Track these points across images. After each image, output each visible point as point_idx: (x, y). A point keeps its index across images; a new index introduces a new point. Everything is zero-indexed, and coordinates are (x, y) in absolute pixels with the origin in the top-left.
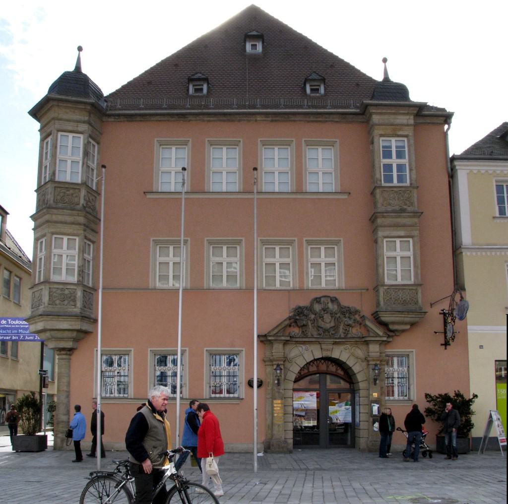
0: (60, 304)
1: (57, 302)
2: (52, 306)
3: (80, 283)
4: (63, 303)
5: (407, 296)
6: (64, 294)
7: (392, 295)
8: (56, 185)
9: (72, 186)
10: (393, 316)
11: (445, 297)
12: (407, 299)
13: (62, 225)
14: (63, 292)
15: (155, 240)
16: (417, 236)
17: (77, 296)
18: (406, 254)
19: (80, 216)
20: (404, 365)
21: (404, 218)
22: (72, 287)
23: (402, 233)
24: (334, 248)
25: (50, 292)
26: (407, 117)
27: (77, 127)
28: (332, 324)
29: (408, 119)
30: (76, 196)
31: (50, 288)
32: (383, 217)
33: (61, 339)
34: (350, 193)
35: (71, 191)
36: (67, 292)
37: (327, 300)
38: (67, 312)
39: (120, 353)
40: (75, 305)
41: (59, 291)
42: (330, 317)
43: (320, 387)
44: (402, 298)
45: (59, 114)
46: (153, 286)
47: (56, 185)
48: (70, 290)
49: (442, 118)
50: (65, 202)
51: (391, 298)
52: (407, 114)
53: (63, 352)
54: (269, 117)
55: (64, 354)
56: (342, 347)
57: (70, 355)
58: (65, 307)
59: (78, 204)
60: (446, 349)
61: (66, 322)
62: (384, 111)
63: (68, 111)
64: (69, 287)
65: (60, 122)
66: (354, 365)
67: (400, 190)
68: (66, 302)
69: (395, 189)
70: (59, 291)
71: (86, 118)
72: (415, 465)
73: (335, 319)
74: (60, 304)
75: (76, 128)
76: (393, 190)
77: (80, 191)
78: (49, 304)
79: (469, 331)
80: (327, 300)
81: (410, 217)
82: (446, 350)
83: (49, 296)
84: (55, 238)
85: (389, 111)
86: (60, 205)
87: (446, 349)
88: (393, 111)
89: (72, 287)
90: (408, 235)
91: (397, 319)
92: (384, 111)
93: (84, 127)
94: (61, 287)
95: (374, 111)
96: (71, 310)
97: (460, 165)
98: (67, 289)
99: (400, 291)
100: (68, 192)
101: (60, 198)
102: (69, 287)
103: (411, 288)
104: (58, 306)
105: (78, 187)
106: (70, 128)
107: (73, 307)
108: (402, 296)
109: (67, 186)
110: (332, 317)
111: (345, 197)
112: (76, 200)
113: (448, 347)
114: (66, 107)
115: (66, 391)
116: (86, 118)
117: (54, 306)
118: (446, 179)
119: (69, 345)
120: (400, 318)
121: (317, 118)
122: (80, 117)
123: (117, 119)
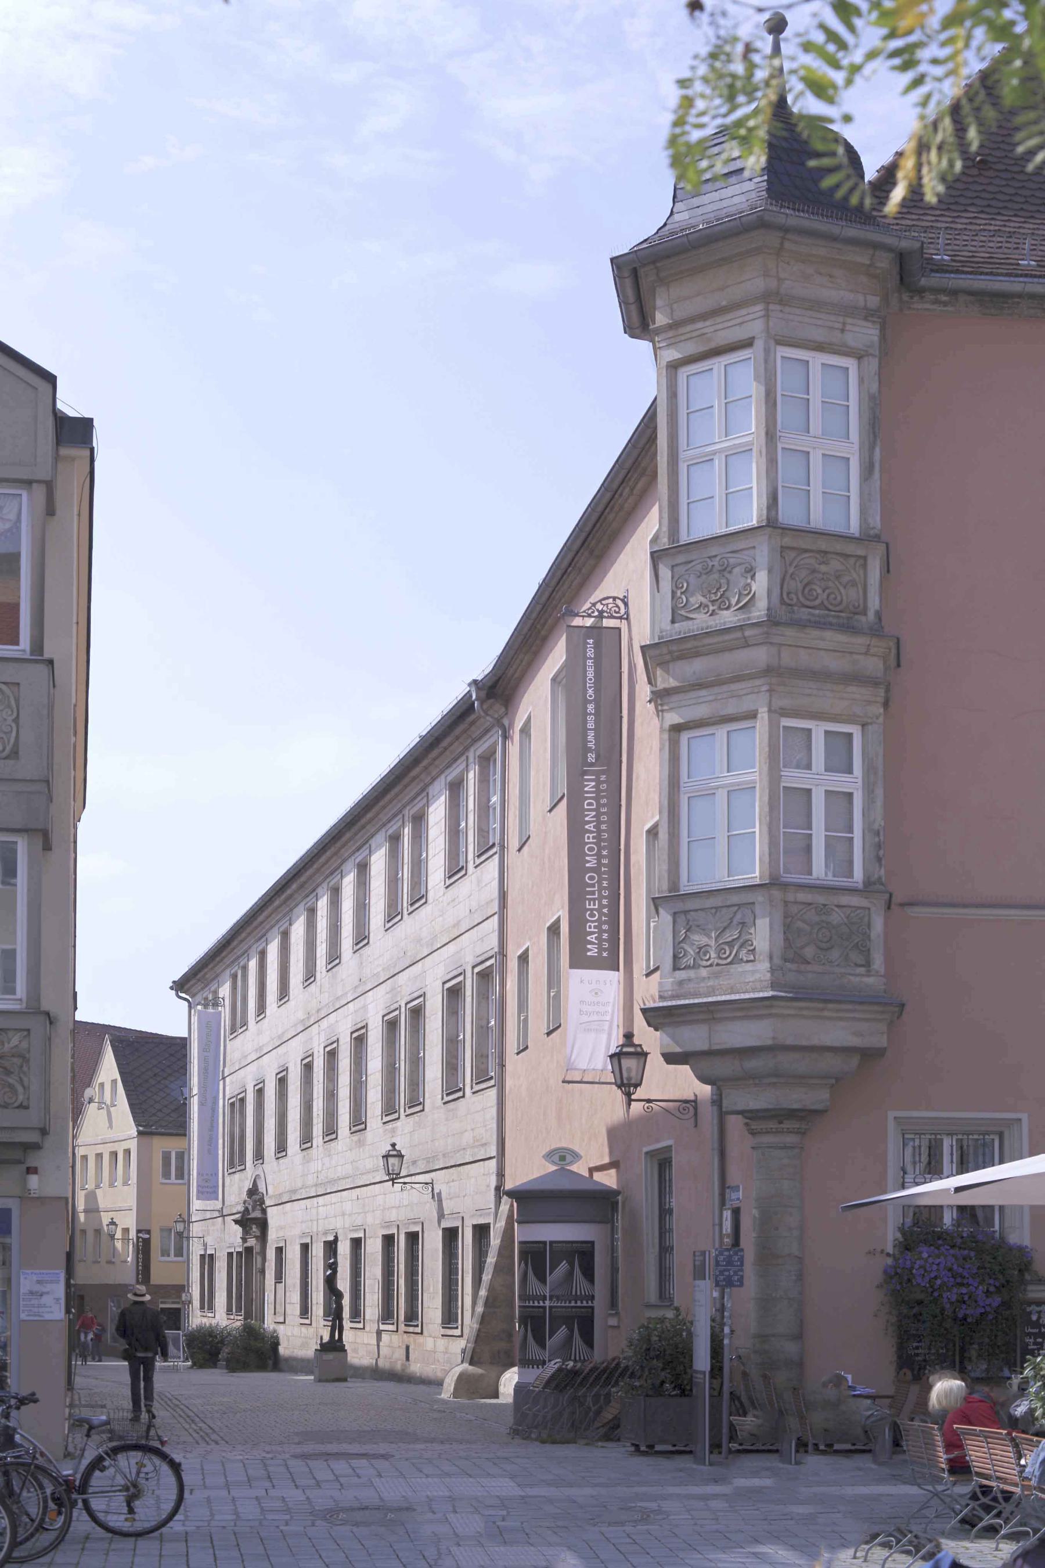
1: (809, 952)
2: (794, 966)
6: (828, 923)
8: (787, 541)
9: (839, 547)
14: (824, 918)
17: (873, 935)
18: (841, 782)
20: (293, 1255)
27: (843, 331)
30: (853, 583)
31: (786, 903)
33: (800, 1080)
35: (835, 564)
36: (836, 917)
39: (983, 1129)
40: (868, 964)
43: (619, 1322)
45: (780, 280)
47: (787, 541)
48: (848, 911)
50: (817, 602)
53: (787, 1125)
55: (790, 1132)
57: (803, 1133)
59: (864, 613)
68: (835, 954)
71: (874, 301)
77: (864, 566)
78: (786, 960)
84: (850, 736)
86: (803, 614)
89: (855, 901)
93: (865, 334)
94: (821, 899)
98: (838, 906)
100: (823, 568)
101: (800, 586)
105: (860, 552)
106: (818, 335)
107: (862, 970)
109: (822, 545)
112: (852, 595)
115: (796, 1257)
116: (874, 301)
117: (803, 967)
119: (814, 1098)
123: (945, 304)
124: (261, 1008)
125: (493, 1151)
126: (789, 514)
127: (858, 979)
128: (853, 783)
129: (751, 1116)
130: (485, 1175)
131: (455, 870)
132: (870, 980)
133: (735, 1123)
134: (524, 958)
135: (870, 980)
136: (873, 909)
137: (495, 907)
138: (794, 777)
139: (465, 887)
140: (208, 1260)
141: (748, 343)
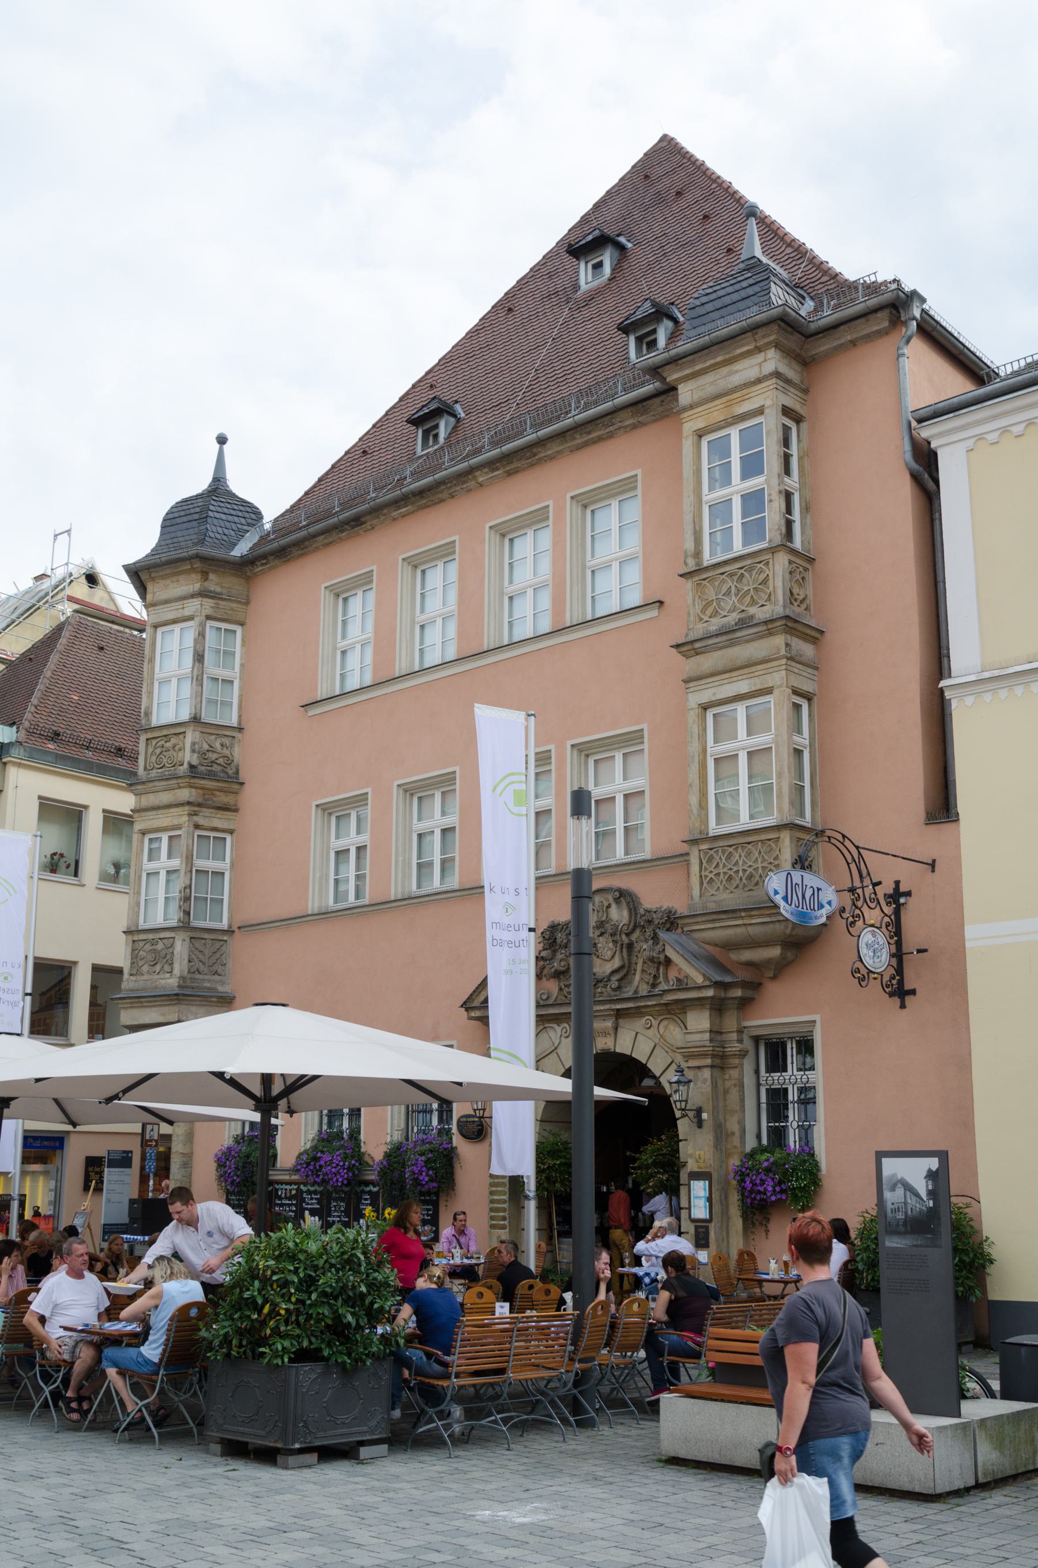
0: (148, 972)
3: (185, 926)
4: (153, 969)
5: (756, 861)
7: (721, 866)
10: (717, 925)
11: (886, 852)
12: (756, 869)
13: (154, 813)
15: (404, 784)
16: (780, 686)
19: (184, 787)
21: (748, 641)
22: (167, 934)
23: (743, 686)
24: (225, 839)
25: (133, 950)
26: (760, 357)
28: (616, 963)
29: (760, 364)
31: (134, 941)
32: (697, 654)
34: (661, 603)
37: (607, 900)
38: (156, 988)
41: (148, 947)
42: (611, 945)
44: (744, 871)
46: (400, 890)
49: (879, 315)
51: (718, 874)
52: (759, 350)
54: (497, 469)
56: (640, 1024)
58: (156, 977)
60: (903, 1006)
61: (156, 1009)
62: (698, 367)
63: (168, 582)
64: (162, 935)
65: (157, 608)
66: (661, 1075)
67: (741, 568)
68: (158, 968)
69: (727, 568)
70: (148, 947)
72: (579, 1441)
73: (622, 948)
74: (148, 972)
75: (181, 611)
76: (723, 574)
78: (131, 975)
79: (968, 944)
80: (607, 900)
81: (759, 637)
82: (904, 1011)
83: (132, 959)
85: (708, 363)
87: (903, 1006)
88: (719, 359)
90: (758, 687)
91: (730, 932)
92: (698, 367)
94: (150, 936)
95: (675, 376)
96: (163, 982)
97: (941, 435)
99: (740, 850)
102: (162, 935)
103: (763, 837)
104: (145, 977)
105: (182, 730)
106: (171, 616)
107: (168, 975)
108: (744, 863)
109: (165, 732)
110: (615, 942)
111: (653, 613)
113: (908, 999)
114: (164, 577)
116: (197, 586)
118: (905, 491)
120: (730, 932)
121: (589, 433)
122: (186, 588)
123: (266, 564)
127: (164, 981)
132: (170, 981)
135: (170, 981)
136: (177, 937)
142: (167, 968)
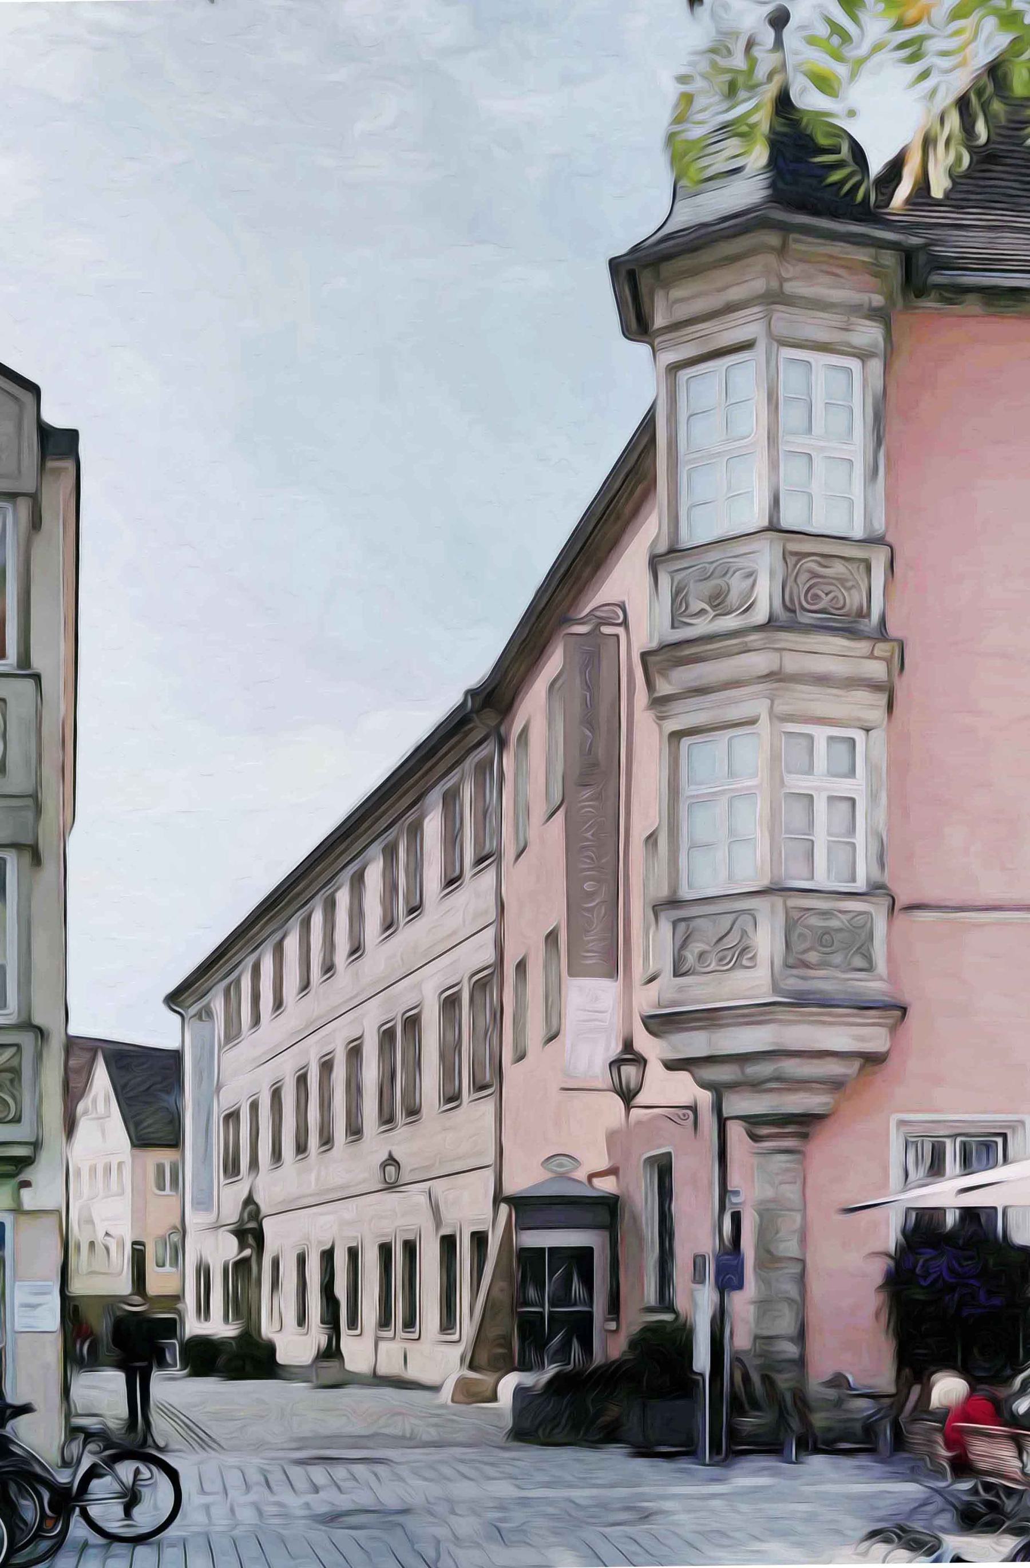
1: (813, 957)
18: (844, 787)
19: (877, 658)
40: (870, 968)
124: (256, 1020)
125: (490, 1158)
126: (789, 519)
128: (856, 787)
129: (752, 1122)
130: (483, 1184)
131: (452, 881)
133: (736, 1131)
134: (521, 967)
137: (492, 916)
138: (799, 783)
139: (462, 897)
140: (204, 1272)
141: (746, 346)
142: (858, 962)
